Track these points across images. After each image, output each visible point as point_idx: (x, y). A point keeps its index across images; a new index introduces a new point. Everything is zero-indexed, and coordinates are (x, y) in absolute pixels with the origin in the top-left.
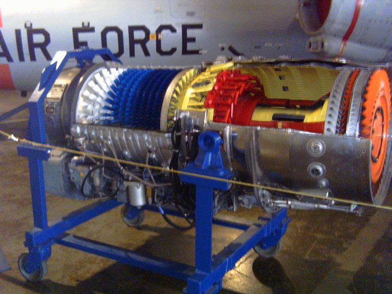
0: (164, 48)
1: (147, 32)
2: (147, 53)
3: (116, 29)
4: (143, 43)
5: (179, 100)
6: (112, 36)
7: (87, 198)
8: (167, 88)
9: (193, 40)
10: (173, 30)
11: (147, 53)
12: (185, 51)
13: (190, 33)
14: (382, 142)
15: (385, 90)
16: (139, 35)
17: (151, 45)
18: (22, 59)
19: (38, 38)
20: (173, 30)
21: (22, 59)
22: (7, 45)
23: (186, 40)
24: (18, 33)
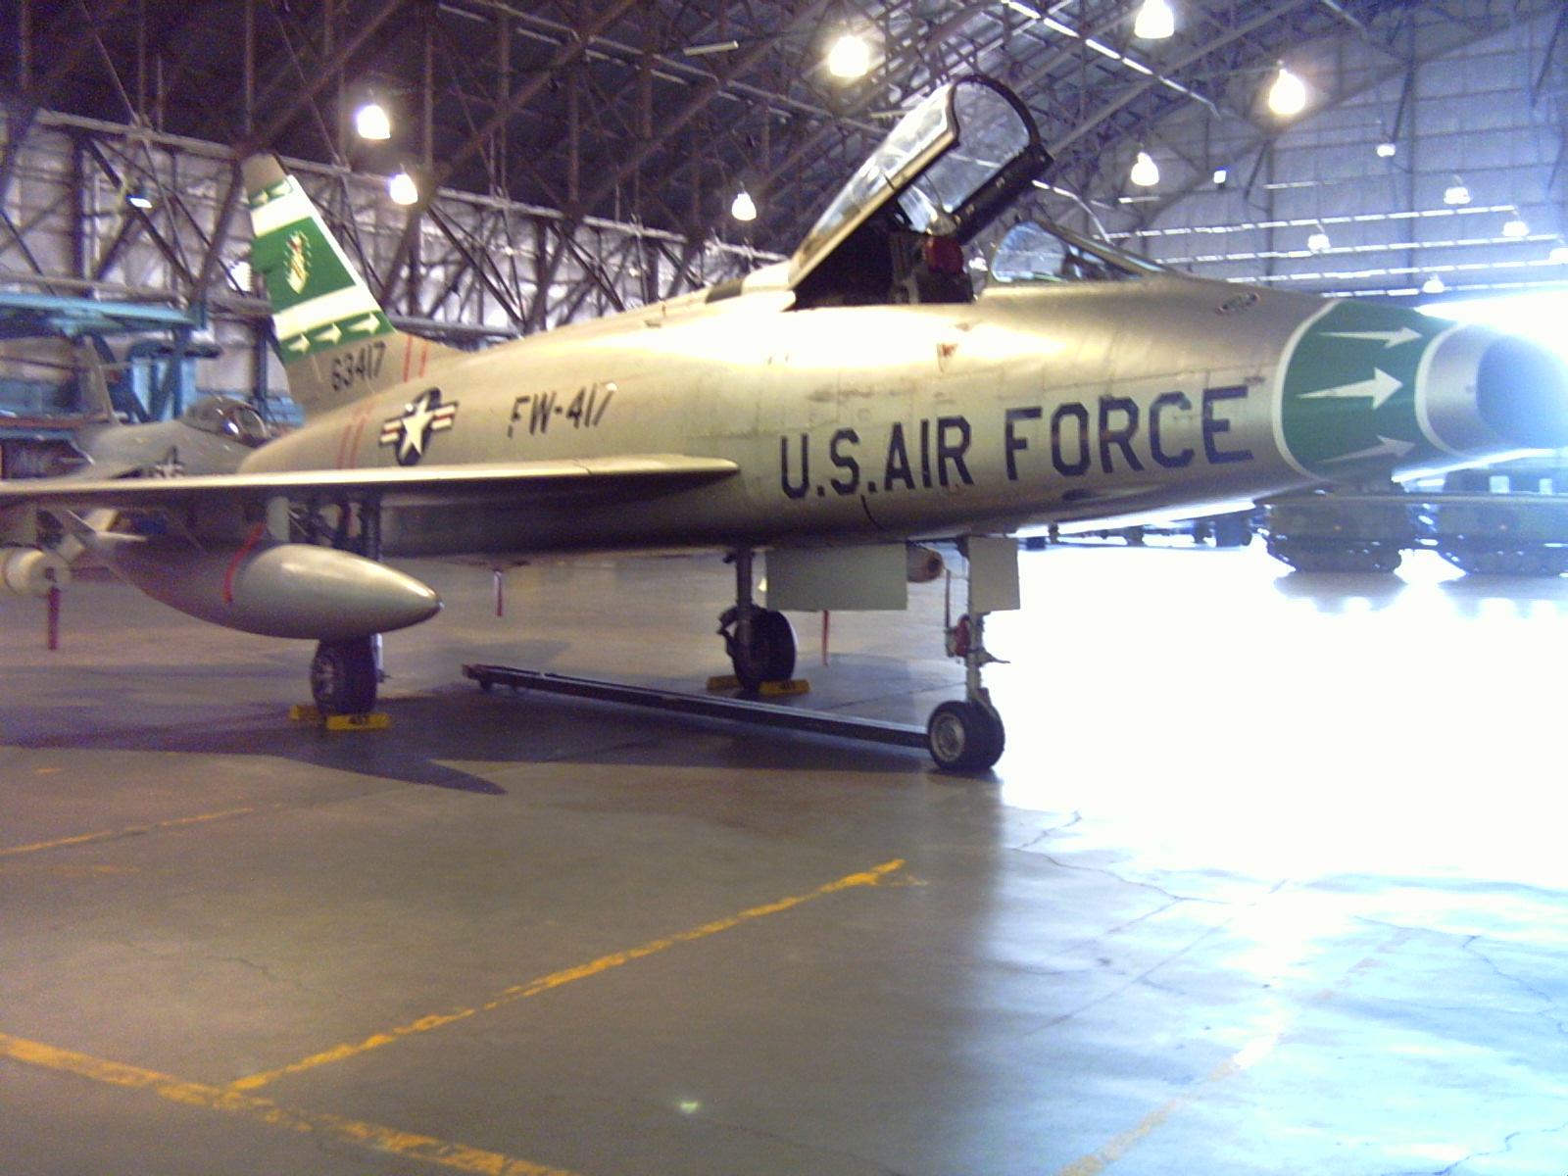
9: (1224, 426)
12: (1213, 456)
13: (1221, 410)
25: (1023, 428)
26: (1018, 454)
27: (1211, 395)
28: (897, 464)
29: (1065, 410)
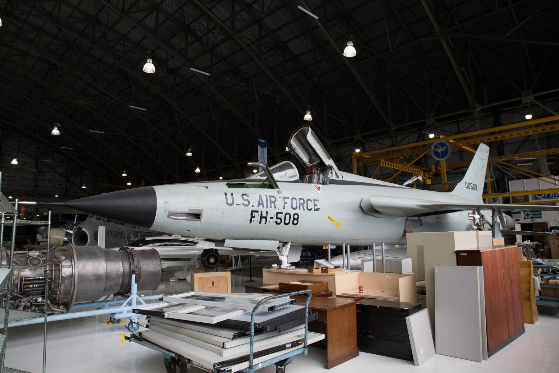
2: (304, 210)
3: (295, 198)
4: (303, 204)
9: (316, 205)
10: (311, 201)
11: (304, 210)
13: (316, 203)
16: (302, 202)
18: (267, 207)
20: (311, 201)
21: (267, 207)
23: (315, 205)
24: (266, 196)
25: (286, 200)
26: (253, 219)
27: (314, 200)
28: (261, 202)
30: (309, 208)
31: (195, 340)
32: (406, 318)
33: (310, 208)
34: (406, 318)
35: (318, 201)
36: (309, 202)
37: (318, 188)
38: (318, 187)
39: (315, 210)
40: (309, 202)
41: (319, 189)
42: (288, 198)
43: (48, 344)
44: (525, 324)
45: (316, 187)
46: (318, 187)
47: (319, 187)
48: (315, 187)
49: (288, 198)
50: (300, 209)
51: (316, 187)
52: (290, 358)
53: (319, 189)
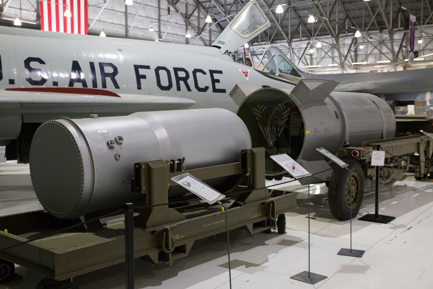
0: (92, 26)
1: (187, 73)
2: (189, 89)
3: (164, 68)
4: (185, 79)
5: (175, 172)
6: (163, 74)
7: (158, 33)
8: (166, 130)
9: (218, 81)
10: (204, 73)
11: (189, 89)
13: (216, 76)
14: (283, 252)
15: (368, 167)
17: (191, 81)
19: (109, 70)
20: (204, 73)
22: (234, 174)
23: (214, 81)
25: (142, 72)
27: (212, 72)
29: (158, 69)
30: (201, 86)
31: (300, 231)
32: (15, 272)
33: (204, 87)
34: (15, 272)
35: (220, 72)
36: (198, 74)
37: (246, 74)
38: (246, 73)
39: (215, 90)
40: (198, 74)
41: (246, 76)
42: (148, 67)
43: (352, 222)
44: (124, 227)
45: (244, 73)
46: (246, 73)
47: (247, 73)
48: (242, 73)
49: (148, 67)
50: (179, 89)
51: (244, 73)
52: (218, 266)
53: (246, 76)
